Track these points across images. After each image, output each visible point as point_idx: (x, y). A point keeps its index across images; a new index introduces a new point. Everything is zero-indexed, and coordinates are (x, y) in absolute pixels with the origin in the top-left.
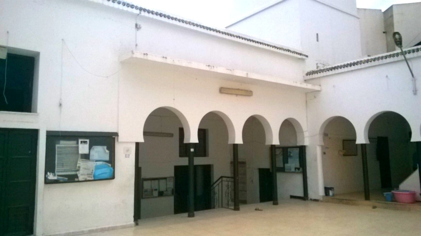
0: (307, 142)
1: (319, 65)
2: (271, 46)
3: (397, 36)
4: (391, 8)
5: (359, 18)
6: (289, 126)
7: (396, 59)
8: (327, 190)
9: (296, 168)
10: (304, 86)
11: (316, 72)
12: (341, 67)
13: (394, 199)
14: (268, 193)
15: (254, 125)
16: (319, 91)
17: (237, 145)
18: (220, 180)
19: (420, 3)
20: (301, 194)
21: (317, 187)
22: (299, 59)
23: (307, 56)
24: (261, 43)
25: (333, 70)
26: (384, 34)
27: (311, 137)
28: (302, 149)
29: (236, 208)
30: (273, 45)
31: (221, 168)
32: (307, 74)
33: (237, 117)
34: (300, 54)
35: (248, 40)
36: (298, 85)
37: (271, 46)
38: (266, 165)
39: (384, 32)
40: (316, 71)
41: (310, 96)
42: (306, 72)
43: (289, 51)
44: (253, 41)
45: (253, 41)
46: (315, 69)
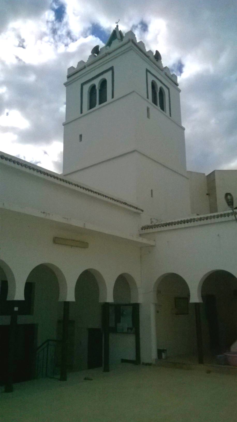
0: (140, 300)
1: (153, 220)
2: (108, 197)
3: (229, 197)
4: (214, 172)
5: (188, 179)
6: (123, 282)
7: (227, 218)
8: (160, 352)
9: (128, 328)
10: (140, 240)
11: (151, 227)
12: (175, 223)
13: (227, 362)
14: (98, 359)
15: (88, 280)
16: (154, 246)
17: (68, 302)
18: (46, 345)
19: (236, 171)
20: (132, 357)
21: (150, 351)
22: (135, 213)
23: (142, 211)
24: (99, 194)
25: (168, 226)
26: (207, 196)
27: (145, 296)
28: (136, 307)
29: (63, 378)
30: (111, 197)
31: (47, 330)
32: (142, 229)
33: (70, 269)
34: (137, 208)
35: (86, 189)
36: (135, 239)
37: (108, 197)
38: (96, 323)
39: (207, 194)
40: (151, 226)
41: (145, 251)
42: (141, 227)
43: (125, 204)
44: (92, 191)
45: (92, 191)
46: (149, 223)
